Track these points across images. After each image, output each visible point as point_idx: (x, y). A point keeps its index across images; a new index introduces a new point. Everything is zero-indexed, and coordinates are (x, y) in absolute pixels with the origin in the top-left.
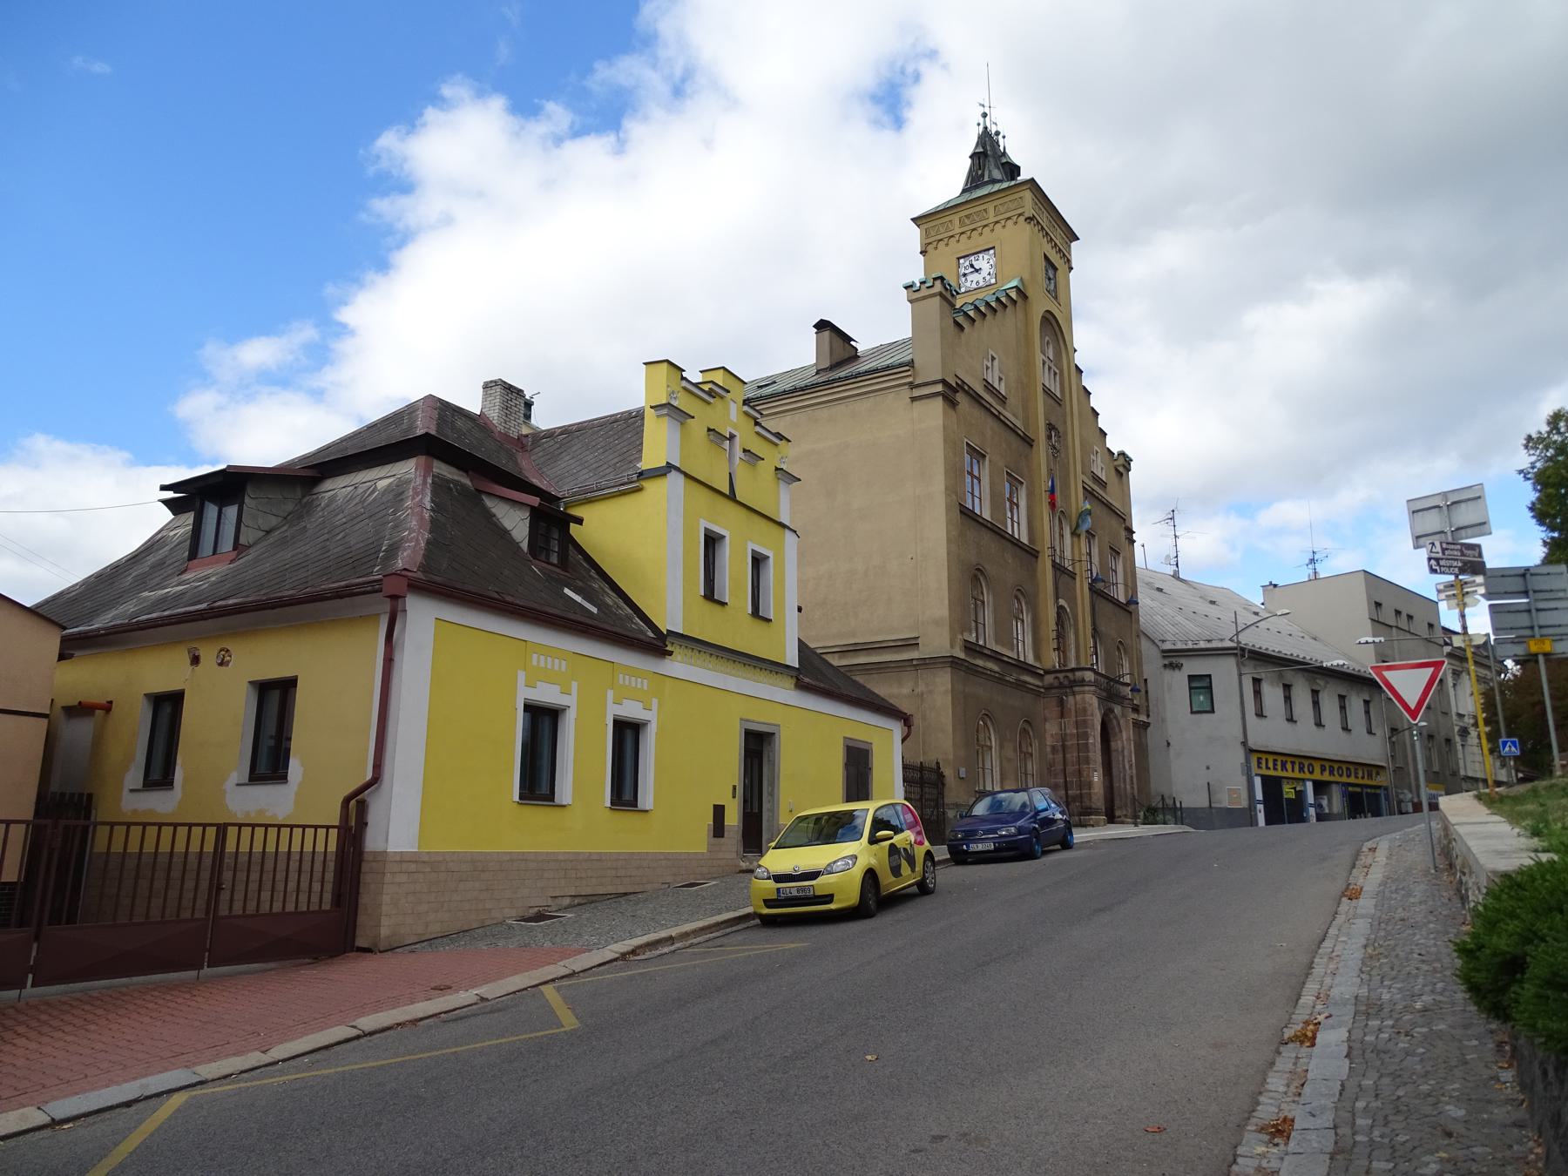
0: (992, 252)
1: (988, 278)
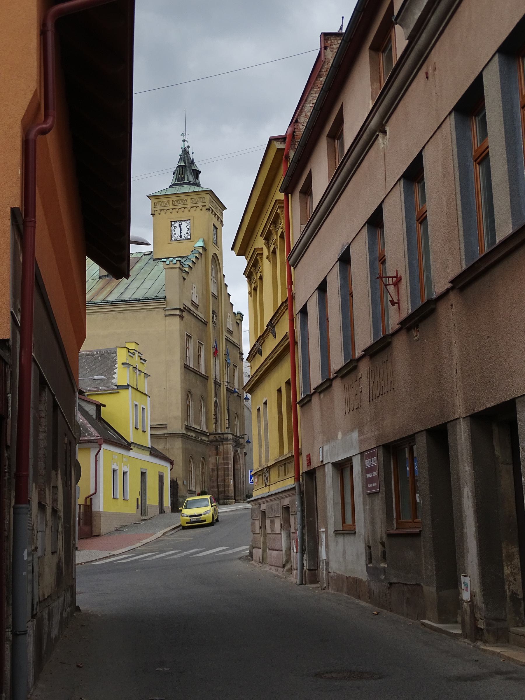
0: (188, 222)
1: (186, 235)
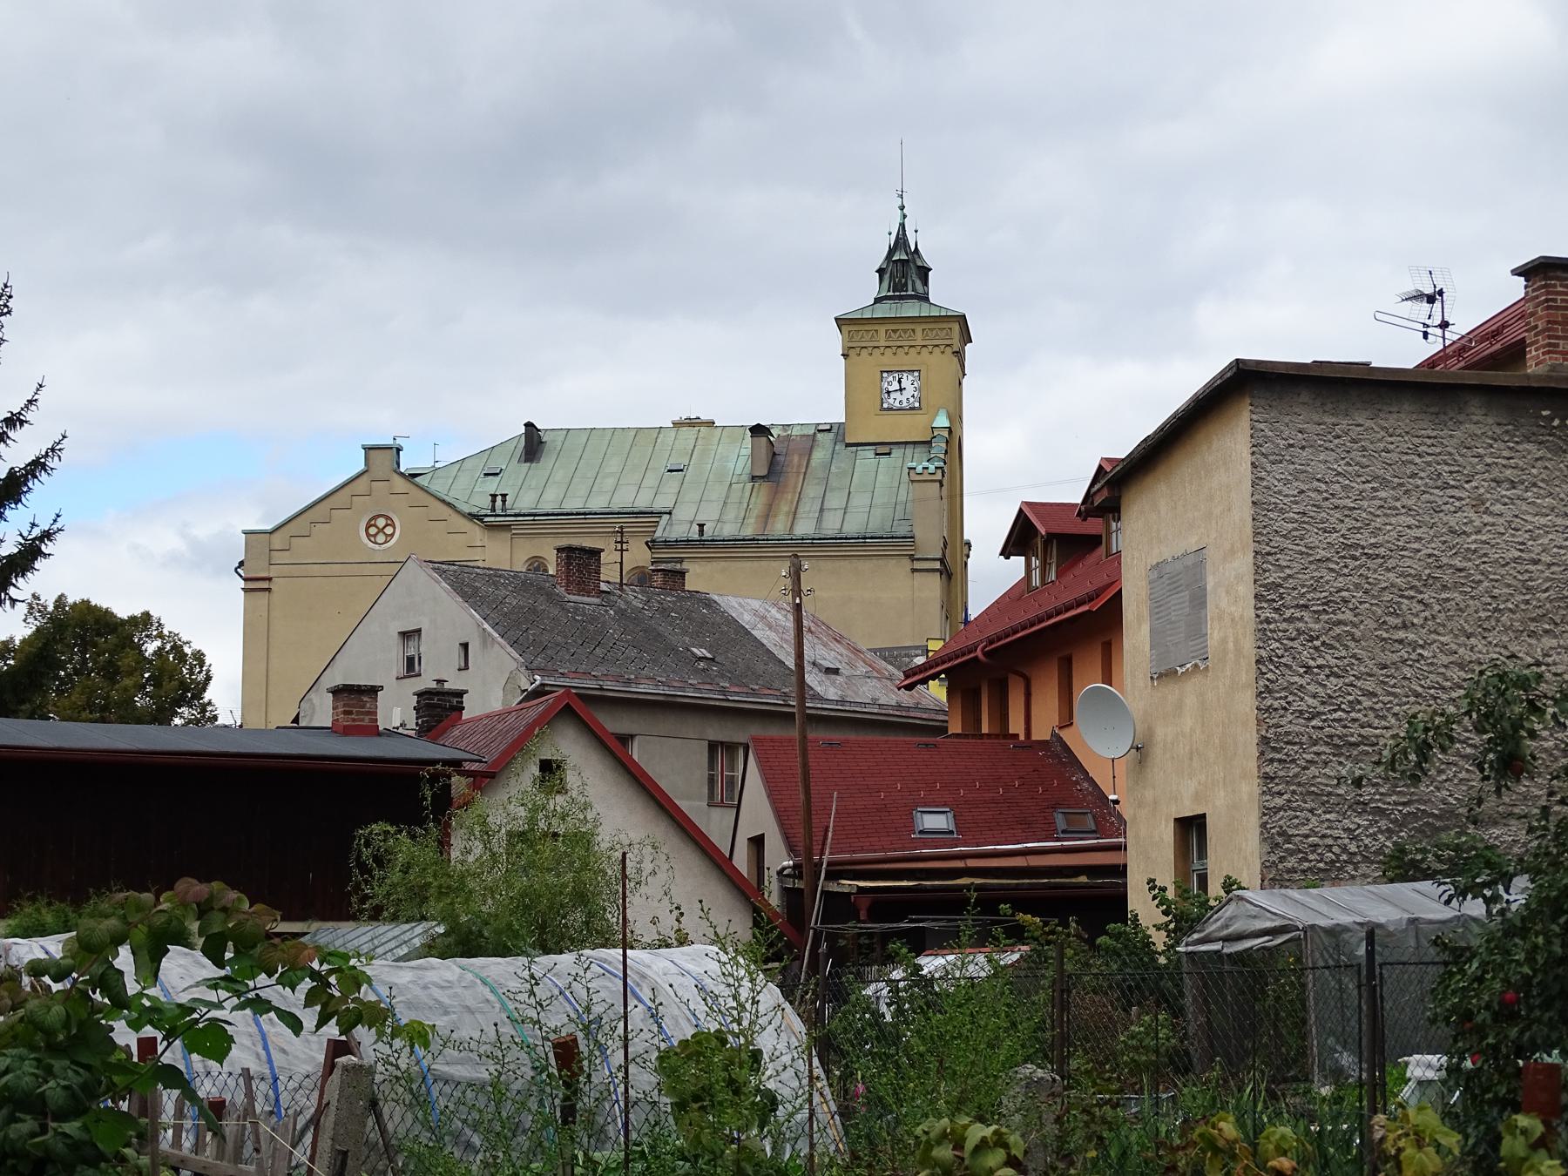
0: (916, 374)
1: (912, 400)
